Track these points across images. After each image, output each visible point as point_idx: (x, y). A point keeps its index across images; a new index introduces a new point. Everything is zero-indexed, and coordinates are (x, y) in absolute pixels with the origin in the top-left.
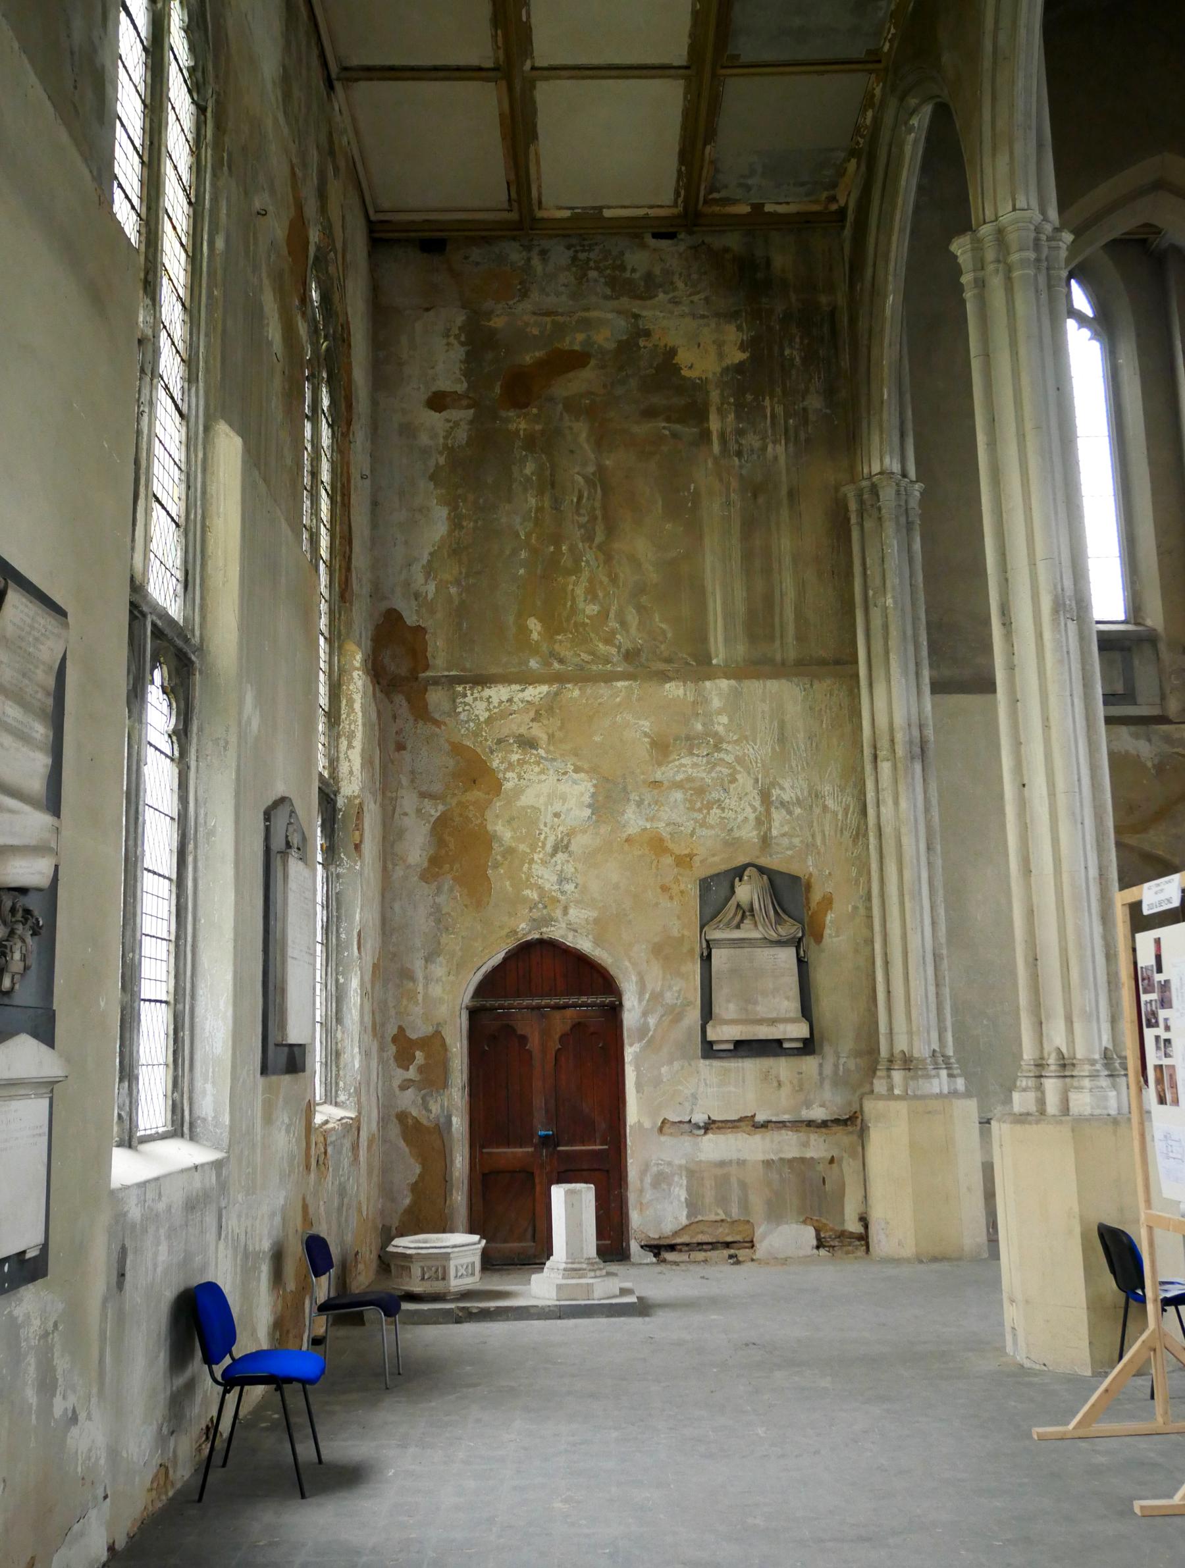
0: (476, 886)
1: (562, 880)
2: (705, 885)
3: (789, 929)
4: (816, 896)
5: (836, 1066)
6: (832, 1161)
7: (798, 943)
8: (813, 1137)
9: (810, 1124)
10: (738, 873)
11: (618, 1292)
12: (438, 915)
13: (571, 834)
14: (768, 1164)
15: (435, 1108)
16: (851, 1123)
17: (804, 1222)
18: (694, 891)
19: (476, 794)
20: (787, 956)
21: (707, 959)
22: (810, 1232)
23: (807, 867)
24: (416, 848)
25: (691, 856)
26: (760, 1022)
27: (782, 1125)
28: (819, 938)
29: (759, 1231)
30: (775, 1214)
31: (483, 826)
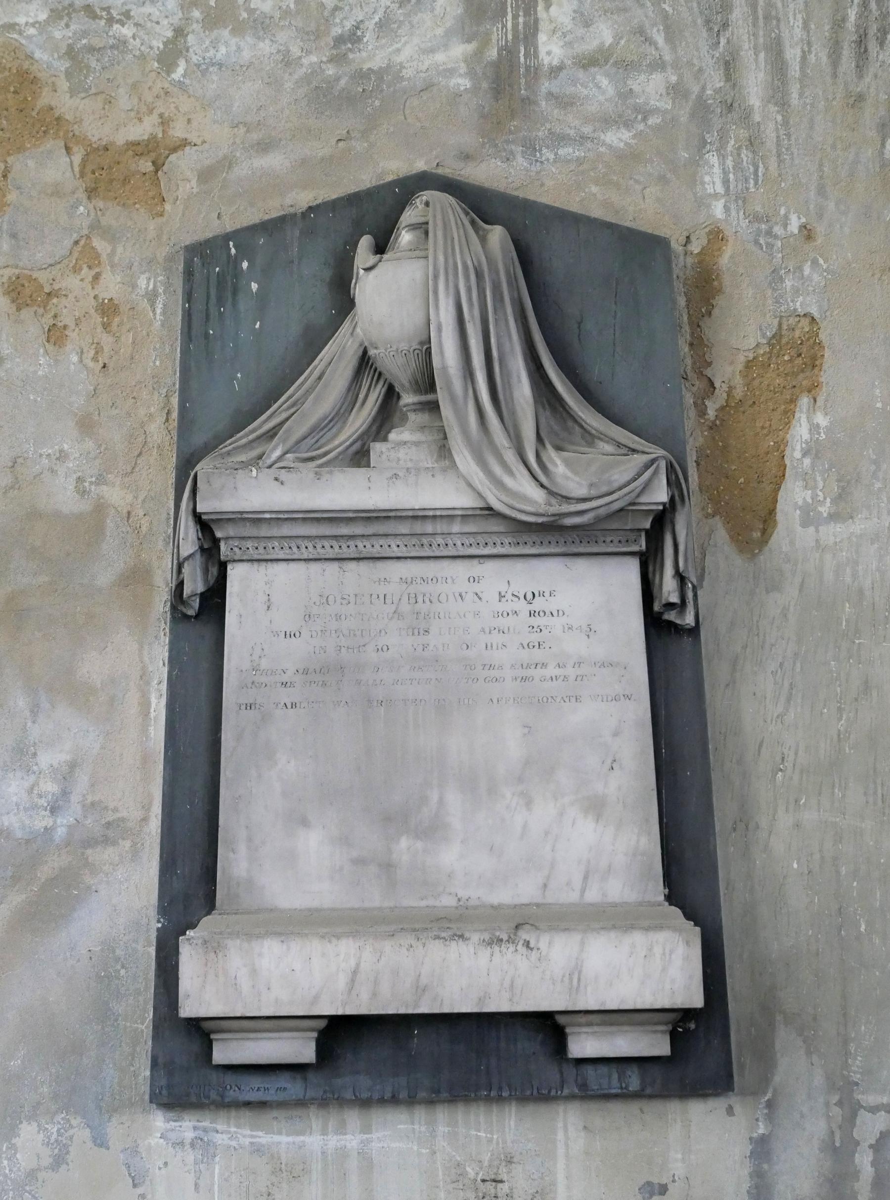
2: (210, 273)
3: (600, 471)
4: (743, 330)
5: (840, 1151)
7: (651, 539)
10: (376, 217)
11: (188, 1009)
18: (152, 297)
20: (598, 600)
21: (203, 612)
23: (698, 200)
25: (157, 152)
28: (752, 524)
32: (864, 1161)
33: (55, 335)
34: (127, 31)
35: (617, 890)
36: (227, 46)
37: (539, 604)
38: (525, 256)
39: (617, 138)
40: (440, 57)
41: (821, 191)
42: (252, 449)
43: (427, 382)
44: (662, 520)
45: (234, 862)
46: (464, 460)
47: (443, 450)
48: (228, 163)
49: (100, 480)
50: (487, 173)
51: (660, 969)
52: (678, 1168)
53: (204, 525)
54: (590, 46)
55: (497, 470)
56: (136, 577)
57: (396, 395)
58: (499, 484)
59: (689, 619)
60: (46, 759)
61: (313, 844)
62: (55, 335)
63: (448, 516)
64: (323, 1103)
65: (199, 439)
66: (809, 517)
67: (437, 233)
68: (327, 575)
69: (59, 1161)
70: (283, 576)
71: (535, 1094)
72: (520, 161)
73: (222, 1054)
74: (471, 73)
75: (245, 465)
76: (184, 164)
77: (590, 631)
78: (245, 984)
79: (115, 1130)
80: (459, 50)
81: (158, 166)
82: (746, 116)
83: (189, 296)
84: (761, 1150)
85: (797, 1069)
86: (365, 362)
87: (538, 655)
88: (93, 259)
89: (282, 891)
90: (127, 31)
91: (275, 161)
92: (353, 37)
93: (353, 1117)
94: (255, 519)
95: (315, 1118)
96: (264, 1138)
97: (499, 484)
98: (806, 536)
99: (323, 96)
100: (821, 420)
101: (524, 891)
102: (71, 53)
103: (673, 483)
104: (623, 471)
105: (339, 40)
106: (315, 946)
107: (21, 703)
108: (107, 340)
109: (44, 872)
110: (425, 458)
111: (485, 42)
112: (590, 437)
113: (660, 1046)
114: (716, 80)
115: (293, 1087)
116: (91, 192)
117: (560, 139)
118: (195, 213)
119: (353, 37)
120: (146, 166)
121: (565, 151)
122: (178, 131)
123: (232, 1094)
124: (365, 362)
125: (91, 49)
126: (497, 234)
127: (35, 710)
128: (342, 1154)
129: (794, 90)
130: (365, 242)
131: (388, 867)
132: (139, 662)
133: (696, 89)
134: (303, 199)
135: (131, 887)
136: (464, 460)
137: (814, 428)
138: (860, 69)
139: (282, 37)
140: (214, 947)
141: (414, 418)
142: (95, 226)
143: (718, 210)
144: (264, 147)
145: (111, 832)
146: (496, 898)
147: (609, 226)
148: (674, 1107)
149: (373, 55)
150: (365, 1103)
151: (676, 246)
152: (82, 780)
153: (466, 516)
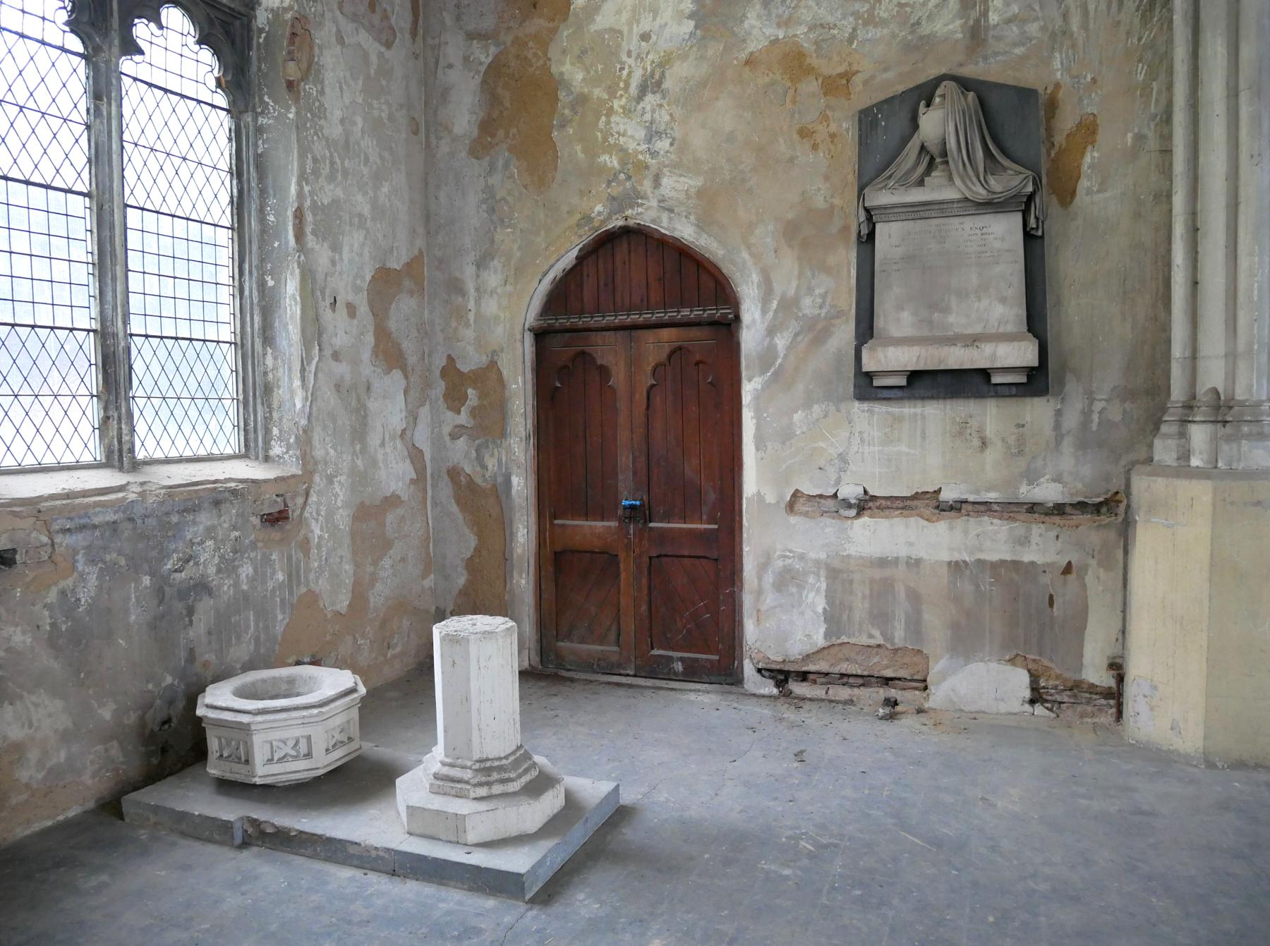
0: (538, 157)
1: (653, 134)
2: (868, 120)
3: (1010, 181)
4: (1067, 121)
5: (1087, 414)
6: (1068, 569)
7: (1026, 205)
8: (1037, 530)
9: (1033, 508)
10: (926, 93)
11: (865, 369)
12: (491, 203)
13: (664, 63)
14: (956, 567)
15: (491, 463)
16: (1108, 509)
17: (1012, 661)
18: (848, 129)
19: (538, 23)
20: (1004, 231)
21: (867, 241)
22: (1019, 681)
24: (463, 114)
25: (847, 76)
26: (952, 340)
27: (984, 508)
28: (1066, 195)
29: (937, 668)
30: (965, 642)
31: (546, 69)
32: (1095, 417)
33: (815, 147)
34: (835, 32)
35: (1010, 328)
36: (873, 33)
37: (985, 230)
38: (982, 102)
39: (1019, 51)
40: (951, 27)
41: (1101, 63)
42: (106, 284)
43: (944, 154)
44: (1031, 197)
45: (879, 322)
46: (958, 181)
47: (951, 179)
48: (873, 77)
49: (832, 197)
50: (969, 71)
51: (1024, 353)
52: (1028, 418)
53: (867, 210)
54: (1009, 14)
55: (970, 184)
56: (845, 229)
57: (933, 159)
58: (970, 189)
59: (1040, 233)
60: (817, 292)
61: (906, 316)
62: (815, 147)
63: (952, 202)
64: (909, 398)
65: (865, 180)
66: (1089, 192)
67: (948, 98)
68: (909, 225)
69: (825, 416)
70: (895, 227)
71: (979, 395)
72: (981, 64)
73: (876, 383)
74: (963, 32)
75: (881, 189)
76: (857, 80)
77: (1003, 239)
78: (883, 360)
79: (843, 407)
80: (958, 23)
81: (848, 81)
82: (1072, 34)
83: (860, 129)
84: (1059, 413)
85: (1073, 387)
86: (923, 148)
87: (983, 249)
88: (826, 118)
89: (895, 332)
90: (835, 32)
91: (889, 75)
92: (918, 23)
93: (919, 403)
94: (885, 208)
95: (907, 403)
96: (890, 409)
97: (970, 189)
98: (1088, 199)
99: (908, 48)
100: (1096, 154)
101: (978, 329)
102: (816, 43)
103: (1035, 183)
104: (1016, 181)
105: (913, 25)
106: (906, 349)
107: (809, 273)
108: (832, 147)
109: (819, 327)
110: (944, 181)
111: (968, 19)
112: (1005, 169)
113: (1023, 379)
114: (1059, 22)
115: (899, 393)
116: (825, 94)
117: (996, 54)
118: (863, 98)
119: (918, 23)
120: (844, 82)
121: (999, 58)
122: (855, 68)
123: (880, 395)
124: (923, 148)
125: (823, 40)
126: (971, 95)
127: (813, 276)
128: (915, 415)
129: (1092, 22)
130: (923, 103)
131: (931, 322)
132: (847, 258)
133: (1051, 28)
134: (901, 88)
135: (846, 332)
136: (958, 181)
137: (1093, 158)
138: (1119, 10)
139: (892, 26)
140: (872, 349)
141: (941, 167)
142: (827, 106)
143: (1059, 75)
144: (886, 70)
145: (840, 314)
146: (966, 332)
147: (1015, 87)
148: (1028, 400)
149: (926, 29)
150: (923, 398)
151: (1041, 91)
152: (829, 300)
153: (959, 201)
